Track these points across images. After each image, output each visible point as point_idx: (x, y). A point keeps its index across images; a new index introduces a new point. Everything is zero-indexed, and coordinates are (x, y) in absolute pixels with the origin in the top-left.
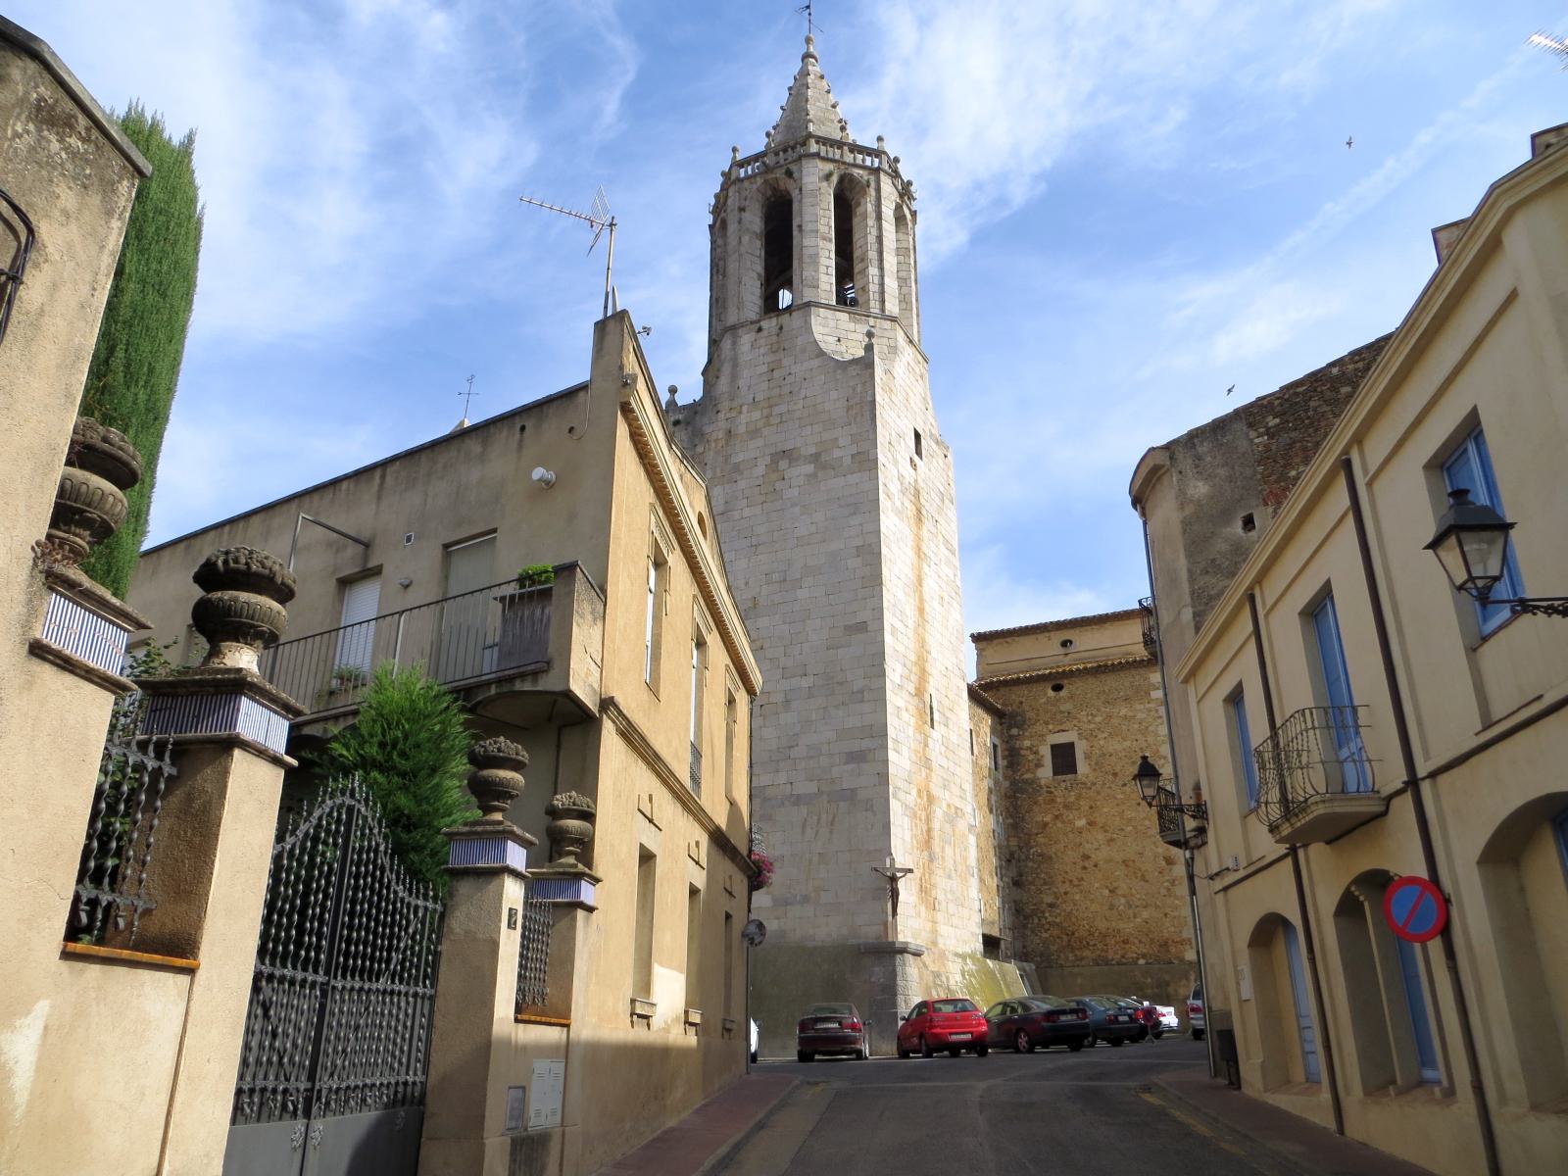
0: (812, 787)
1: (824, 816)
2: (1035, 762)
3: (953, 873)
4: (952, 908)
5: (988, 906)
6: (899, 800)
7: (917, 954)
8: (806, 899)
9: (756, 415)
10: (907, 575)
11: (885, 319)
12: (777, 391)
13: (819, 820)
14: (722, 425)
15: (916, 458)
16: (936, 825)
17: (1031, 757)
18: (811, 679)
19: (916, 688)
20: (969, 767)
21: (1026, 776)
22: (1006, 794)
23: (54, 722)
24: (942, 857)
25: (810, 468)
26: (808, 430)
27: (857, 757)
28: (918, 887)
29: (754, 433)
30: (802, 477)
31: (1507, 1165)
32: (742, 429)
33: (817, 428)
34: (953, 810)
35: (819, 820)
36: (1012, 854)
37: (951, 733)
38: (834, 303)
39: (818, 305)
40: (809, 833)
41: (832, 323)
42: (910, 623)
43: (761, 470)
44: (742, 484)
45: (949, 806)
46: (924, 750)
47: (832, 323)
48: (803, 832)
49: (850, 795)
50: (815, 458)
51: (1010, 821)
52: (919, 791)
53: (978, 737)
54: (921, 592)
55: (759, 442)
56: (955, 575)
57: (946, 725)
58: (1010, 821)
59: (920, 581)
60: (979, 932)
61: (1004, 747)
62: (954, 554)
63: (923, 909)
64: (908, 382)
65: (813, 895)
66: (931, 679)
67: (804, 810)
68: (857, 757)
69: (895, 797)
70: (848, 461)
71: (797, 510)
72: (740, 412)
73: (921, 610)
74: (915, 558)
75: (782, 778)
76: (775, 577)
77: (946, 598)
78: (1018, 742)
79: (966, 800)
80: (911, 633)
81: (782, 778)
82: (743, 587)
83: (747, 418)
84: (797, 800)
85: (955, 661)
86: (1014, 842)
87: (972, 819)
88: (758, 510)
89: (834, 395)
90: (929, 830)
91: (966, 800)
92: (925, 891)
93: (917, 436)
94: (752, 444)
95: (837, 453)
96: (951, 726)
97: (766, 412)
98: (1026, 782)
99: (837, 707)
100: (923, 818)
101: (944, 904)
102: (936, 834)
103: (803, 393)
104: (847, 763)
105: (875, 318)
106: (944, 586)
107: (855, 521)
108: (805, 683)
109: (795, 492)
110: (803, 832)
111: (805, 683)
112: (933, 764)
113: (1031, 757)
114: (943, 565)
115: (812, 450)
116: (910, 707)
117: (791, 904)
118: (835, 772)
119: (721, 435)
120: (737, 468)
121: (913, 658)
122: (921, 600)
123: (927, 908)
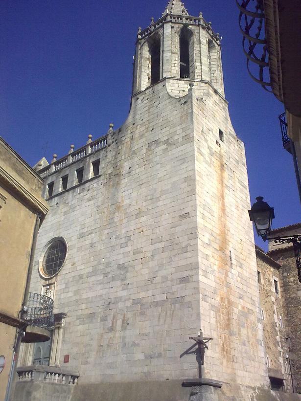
0: (164, 297)
1: (168, 312)
2: (297, 288)
3: (247, 343)
4: (246, 362)
5: (273, 362)
6: (207, 302)
7: (217, 386)
8: (160, 355)
9: (143, 128)
10: (213, 192)
11: (202, 82)
12: (152, 116)
13: (166, 313)
14: (129, 135)
15: (220, 141)
16: (234, 317)
17: (294, 286)
18: (164, 243)
19: (219, 247)
20: (257, 289)
21: (293, 296)
22: (283, 306)
23: (42, 313)
24: (239, 333)
25: (165, 146)
26: (164, 130)
27: (184, 280)
28: (221, 349)
29: (141, 136)
30: (161, 151)
31: (298, 222)
32: (137, 136)
33: (168, 129)
34: (246, 310)
35: (166, 313)
36: (288, 336)
37: (244, 271)
38: (179, 77)
39: (169, 78)
40: (162, 320)
41: (176, 85)
42: (216, 215)
43: (144, 151)
44: (136, 159)
45: (243, 307)
46: (225, 278)
47: (176, 85)
48: (159, 320)
49: (180, 300)
50: (167, 142)
51: (286, 318)
52: (222, 298)
53: (264, 275)
54: (223, 202)
55: (144, 140)
56: (246, 198)
57: (241, 267)
58: (286, 318)
59: (223, 197)
60: (266, 375)
61: (281, 282)
62: (245, 188)
63: (225, 361)
64: (215, 109)
65: (163, 353)
66: (230, 243)
67: (160, 309)
68: (184, 280)
69: (204, 300)
70: (180, 140)
71: (159, 166)
72: (137, 129)
73: (224, 210)
74: (219, 186)
75: (150, 293)
76: (149, 198)
77: (241, 207)
78: (287, 279)
79: (255, 305)
80: (216, 219)
81: (150, 293)
82: (135, 204)
83: (140, 130)
84: (157, 304)
85: (247, 237)
86: (288, 329)
87: (260, 316)
88: (143, 168)
89: (175, 113)
90: (229, 319)
91: (255, 305)
92: (225, 351)
93: (221, 133)
94: (141, 141)
95: (176, 138)
96: (244, 268)
97: (147, 126)
98: (292, 298)
99: (175, 256)
100: (225, 312)
101: (240, 359)
102: (234, 322)
103: (162, 115)
104: (179, 284)
105: (197, 82)
106: (239, 201)
107: (184, 166)
108: (160, 245)
109: (157, 159)
110: (159, 320)
111: (160, 245)
112: (232, 285)
113: (294, 286)
114: (238, 192)
115: (165, 138)
116: (216, 256)
117: (153, 358)
118: (174, 289)
119: (128, 140)
120: (134, 153)
121: (218, 232)
122: (223, 205)
123: (227, 360)
